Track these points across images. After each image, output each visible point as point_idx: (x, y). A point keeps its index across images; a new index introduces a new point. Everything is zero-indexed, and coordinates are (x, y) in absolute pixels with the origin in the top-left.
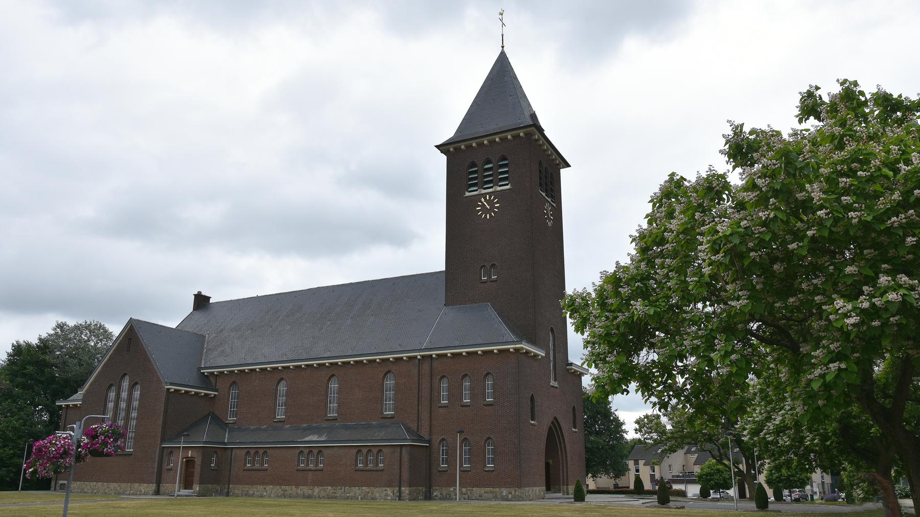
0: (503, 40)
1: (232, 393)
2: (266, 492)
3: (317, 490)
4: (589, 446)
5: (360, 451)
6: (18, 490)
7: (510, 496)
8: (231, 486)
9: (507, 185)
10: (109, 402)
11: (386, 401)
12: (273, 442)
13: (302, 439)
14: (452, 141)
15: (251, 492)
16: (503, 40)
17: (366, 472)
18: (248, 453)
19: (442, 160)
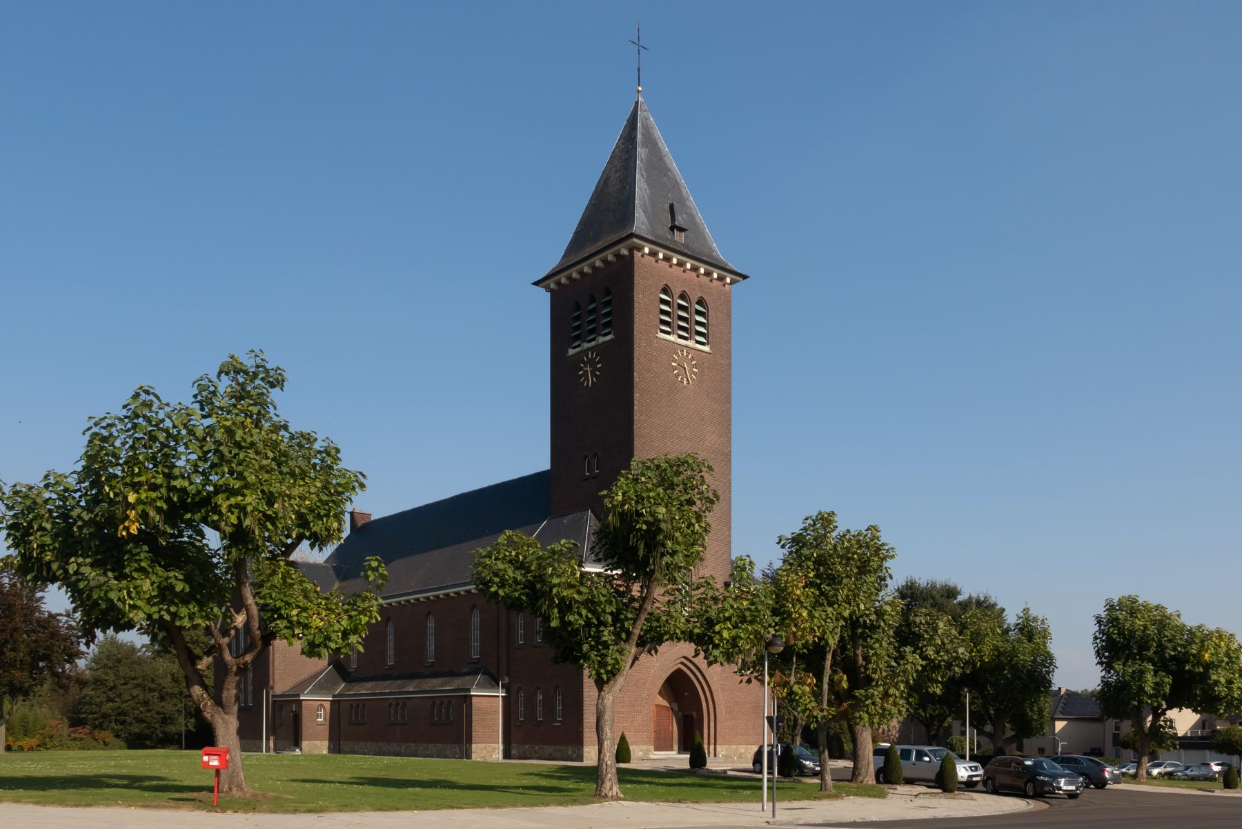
0: (639, 78)
1: (429, 627)
2: (367, 749)
3: (404, 747)
4: (191, 699)
5: (434, 703)
6: (618, 761)
7: (574, 755)
8: (341, 742)
9: (609, 333)
10: (430, 635)
11: (474, 643)
12: (420, 691)
13: (442, 687)
14: (561, 268)
15: (356, 749)
16: (639, 78)
17: (717, 734)
18: (434, 703)
19: (543, 299)
